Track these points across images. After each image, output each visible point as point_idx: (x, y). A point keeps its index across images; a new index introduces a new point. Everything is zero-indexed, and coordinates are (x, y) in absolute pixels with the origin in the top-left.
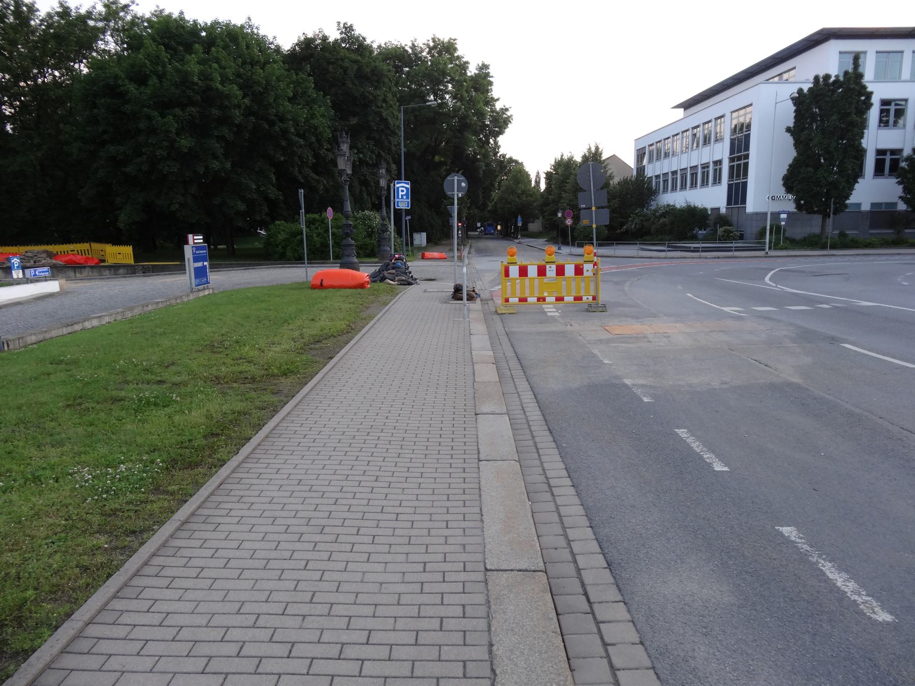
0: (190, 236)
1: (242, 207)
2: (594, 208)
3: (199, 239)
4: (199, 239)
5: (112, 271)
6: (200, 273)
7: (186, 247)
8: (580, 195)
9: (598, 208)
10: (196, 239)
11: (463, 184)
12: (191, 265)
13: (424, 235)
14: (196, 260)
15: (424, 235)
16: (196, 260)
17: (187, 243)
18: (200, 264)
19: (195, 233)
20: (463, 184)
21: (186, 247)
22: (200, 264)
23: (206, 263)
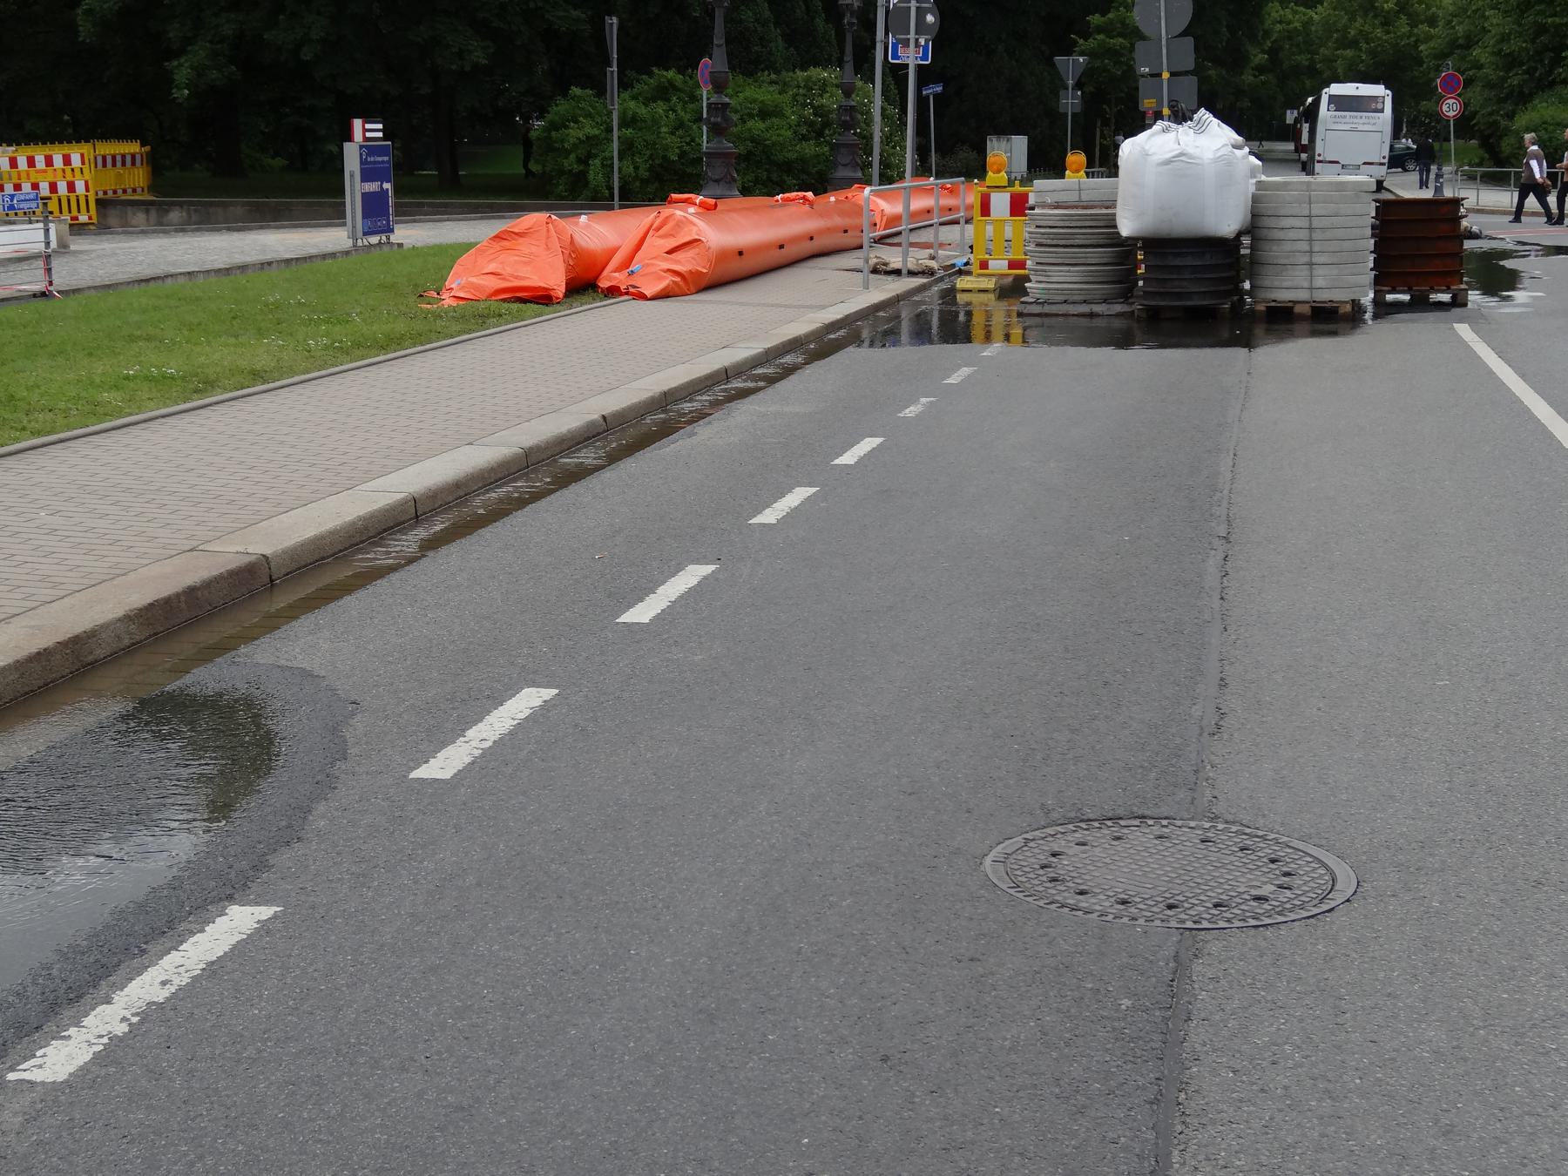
0: (357, 124)
1: (480, 53)
2: (1166, 75)
3: (376, 130)
4: (376, 130)
5: (153, 213)
6: (374, 207)
7: (347, 145)
8: (1139, 45)
9: (1172, 74)
10: (366, 131)
11: (930, 18)
12: (355, 188)
13: (1020, 143)
14: (367, 176)
15: (1020, 143)
16: (367, 176)
17: (350, 138)
18: (372, 187)
19: (368, 117)
20: (930, 18)
21: (347, 145)
22: (372, 187)
23: (387, 186)
